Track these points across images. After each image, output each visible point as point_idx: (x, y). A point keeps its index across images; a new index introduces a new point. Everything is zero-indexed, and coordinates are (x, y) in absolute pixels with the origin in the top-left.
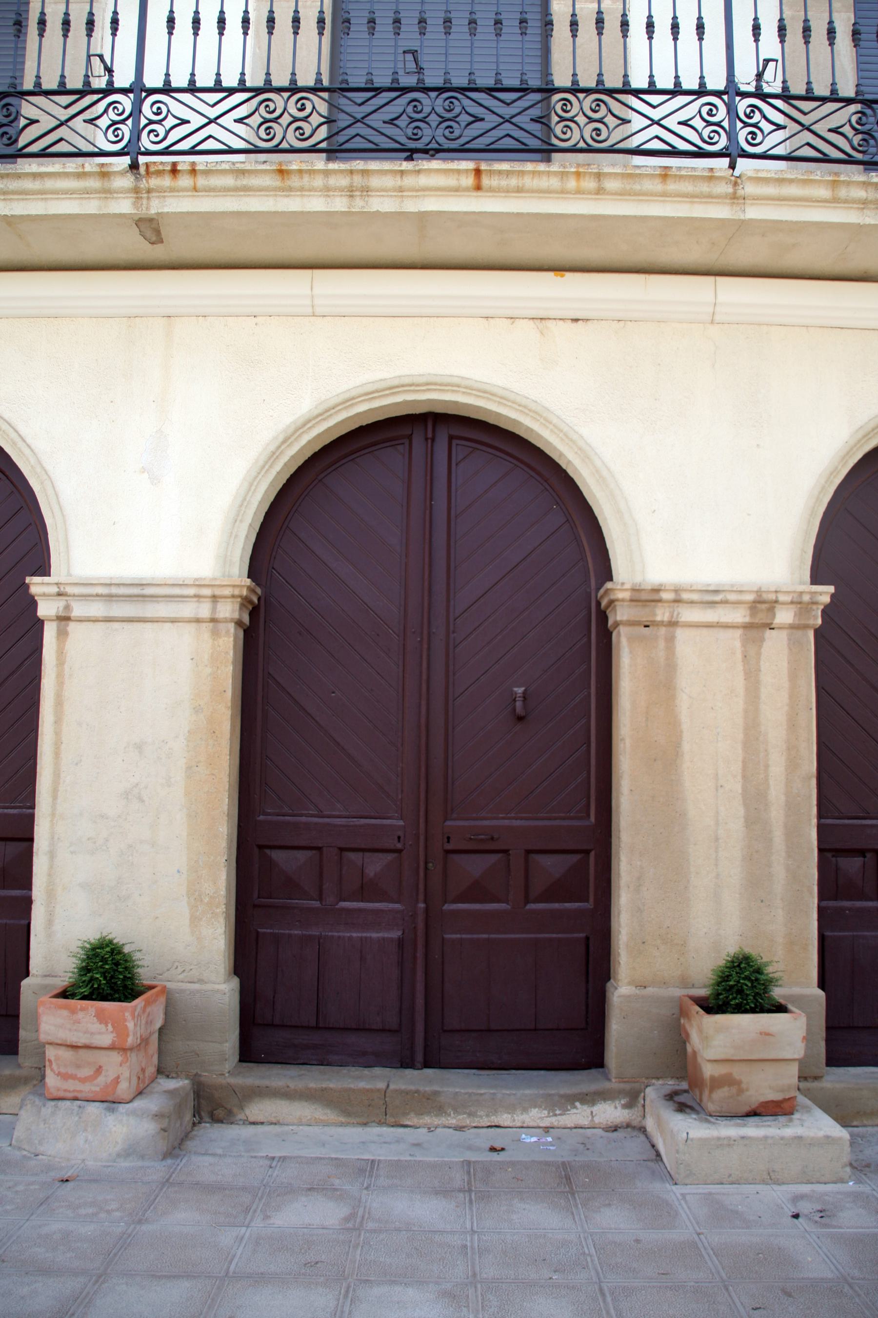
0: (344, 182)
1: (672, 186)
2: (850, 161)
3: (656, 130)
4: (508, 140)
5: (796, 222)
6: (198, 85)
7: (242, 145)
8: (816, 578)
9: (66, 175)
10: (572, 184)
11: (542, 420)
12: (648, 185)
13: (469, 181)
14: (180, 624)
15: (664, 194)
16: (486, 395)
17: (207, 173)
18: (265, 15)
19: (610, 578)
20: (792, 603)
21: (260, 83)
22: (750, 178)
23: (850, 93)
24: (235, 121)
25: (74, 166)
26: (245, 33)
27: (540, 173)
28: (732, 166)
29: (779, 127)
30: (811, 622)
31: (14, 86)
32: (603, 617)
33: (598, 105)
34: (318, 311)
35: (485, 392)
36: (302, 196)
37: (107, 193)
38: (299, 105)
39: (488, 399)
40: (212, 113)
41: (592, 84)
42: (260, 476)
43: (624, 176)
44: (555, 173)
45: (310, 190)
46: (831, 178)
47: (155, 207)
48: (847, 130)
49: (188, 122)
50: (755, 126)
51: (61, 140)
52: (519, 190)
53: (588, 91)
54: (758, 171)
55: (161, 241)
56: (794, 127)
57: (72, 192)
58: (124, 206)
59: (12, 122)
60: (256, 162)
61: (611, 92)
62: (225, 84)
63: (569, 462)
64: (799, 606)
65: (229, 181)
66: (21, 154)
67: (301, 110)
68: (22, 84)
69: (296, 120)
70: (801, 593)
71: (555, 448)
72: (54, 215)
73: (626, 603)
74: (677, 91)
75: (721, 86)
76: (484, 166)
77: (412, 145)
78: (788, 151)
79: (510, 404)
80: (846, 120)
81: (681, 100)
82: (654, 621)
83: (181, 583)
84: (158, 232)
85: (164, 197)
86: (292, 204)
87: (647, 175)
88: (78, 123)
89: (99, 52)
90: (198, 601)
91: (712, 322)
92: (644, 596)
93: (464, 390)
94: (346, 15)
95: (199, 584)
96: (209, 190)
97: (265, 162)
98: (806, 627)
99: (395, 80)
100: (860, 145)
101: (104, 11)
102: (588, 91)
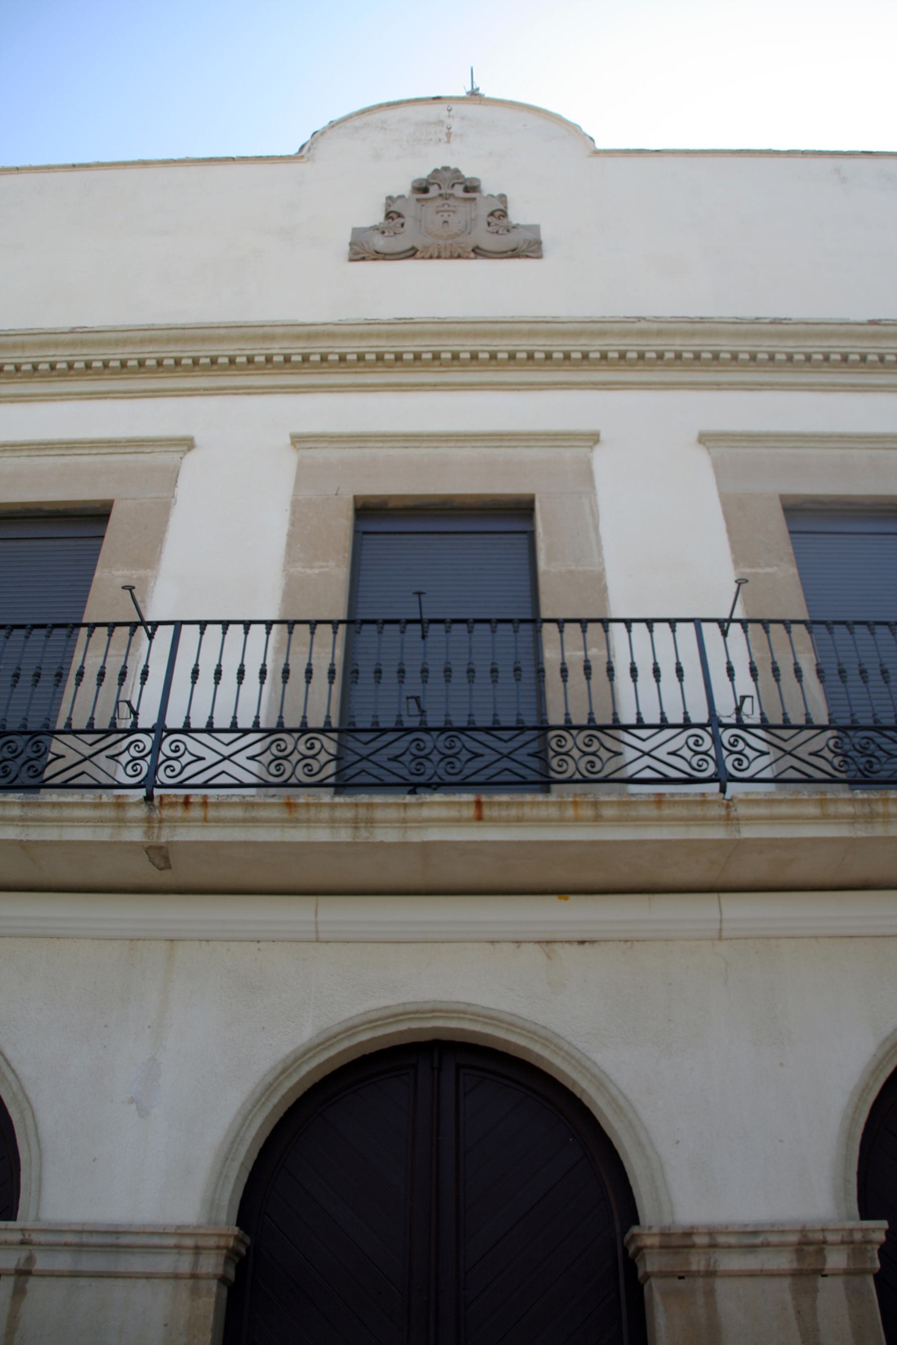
0: (349, 814)
1: (667, 811)
2: (834, 780)
3: (647, 760)
4: (506, 737)
5: (792, 839)
6: (216, 726)
7: (254, 780)
8: (866, 1213)
9: (83, 805)
10: (570, 812)
11: (552, 1047)
12: (644, 811)
13: (470, 812)
14: (156, 1281)
15: (660, 819)
16: (493, 1022)
17: (218, 805)
18: (281, 667)
19: (636, 1221)
20: (843, 1243)
21: (273, 725)
22: (741, 801)
23: (824, 720)
24: (248, 758)
25: (92, 796)
26: (262, 683)
27: (539, 804)
28: (723, 790)
29: (763, 753)
30: (868, 1266)
31: (47, 726)
32: (631, 1266)
33: (591, 740)
34: (322, 936)
35: (492, 1018)
36: (308, 827)
37: (121, 822)
38: (308, 745)
39: (496, 1026)
40: (227, 751)
41: (584, 721)
42: (256, 1110)
43: (619, 803)
44: (554, 803)
45: (316, 822)
46: (818, 797)
47: (166, 835)
48: (826, 753)
49: (203, 759)
50: (740, 753)
51: (83, 773)
52: (519, 820)
53: (580, 728)
54: (747, 794)
55: (170, 867)
56: (775, 753)
57: (86, 820)
58: (136, 835)
59: (40, 757)
60: (266, 796)
61: (602, 728)
62: (240, 725)
63: (583, 1090)
64: (851, 1246)
65: (239, 813)
66: (44, 785)
67: (309, 749)
68: (55, 722)
69: (305, 757)
70: (851, 1231)
71: (568, 1076)
72: (68, 841)
73: (656, 1251)
74: (663, 725)
75: (704, 718)
76: (484, 799)
77: (415, 779)
78: (776, 774)
79: (519, 1030)
80: (824, 744)
81: (668, 733)
82: (689, 1271)
83: (161, 1231)
84: (166, 859)
85: (175, 827)
86: (298, 835)
87: (642, 802)
88: (101, 759)
89: (128, 699)
90: (179, 1253)
91: (720, 938)
92: (675, 1241)
93: (471, 1017)
94: (355, 667)
95: (181, 1232)
96: (218, 820)
97: (274, 796)
98: (862, 1272)
99: (400, 722)
100: (841, 766)
101: (138, 662)
102: (580, 728)
